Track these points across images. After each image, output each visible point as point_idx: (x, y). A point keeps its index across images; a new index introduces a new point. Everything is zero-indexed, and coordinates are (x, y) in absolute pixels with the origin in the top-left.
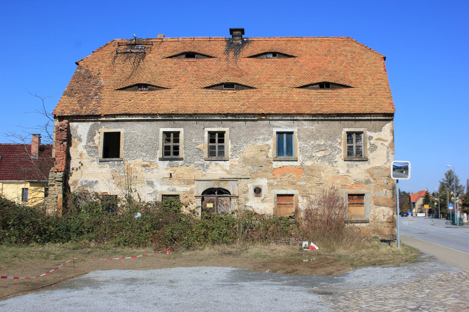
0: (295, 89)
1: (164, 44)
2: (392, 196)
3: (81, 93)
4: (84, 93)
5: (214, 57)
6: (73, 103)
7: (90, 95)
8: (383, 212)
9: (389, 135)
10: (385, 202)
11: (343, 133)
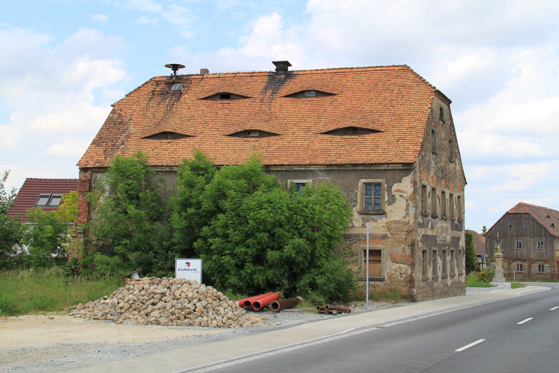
0: (320, 135)
1: (204, 81)
2: (410, 253)
3: (109, 142)
4: (111, 142)
5: (249, 98)
6: (98, 153)
7: (117, 144)
8: (401, 270)
9: (409, 187)
11: (360, 184)
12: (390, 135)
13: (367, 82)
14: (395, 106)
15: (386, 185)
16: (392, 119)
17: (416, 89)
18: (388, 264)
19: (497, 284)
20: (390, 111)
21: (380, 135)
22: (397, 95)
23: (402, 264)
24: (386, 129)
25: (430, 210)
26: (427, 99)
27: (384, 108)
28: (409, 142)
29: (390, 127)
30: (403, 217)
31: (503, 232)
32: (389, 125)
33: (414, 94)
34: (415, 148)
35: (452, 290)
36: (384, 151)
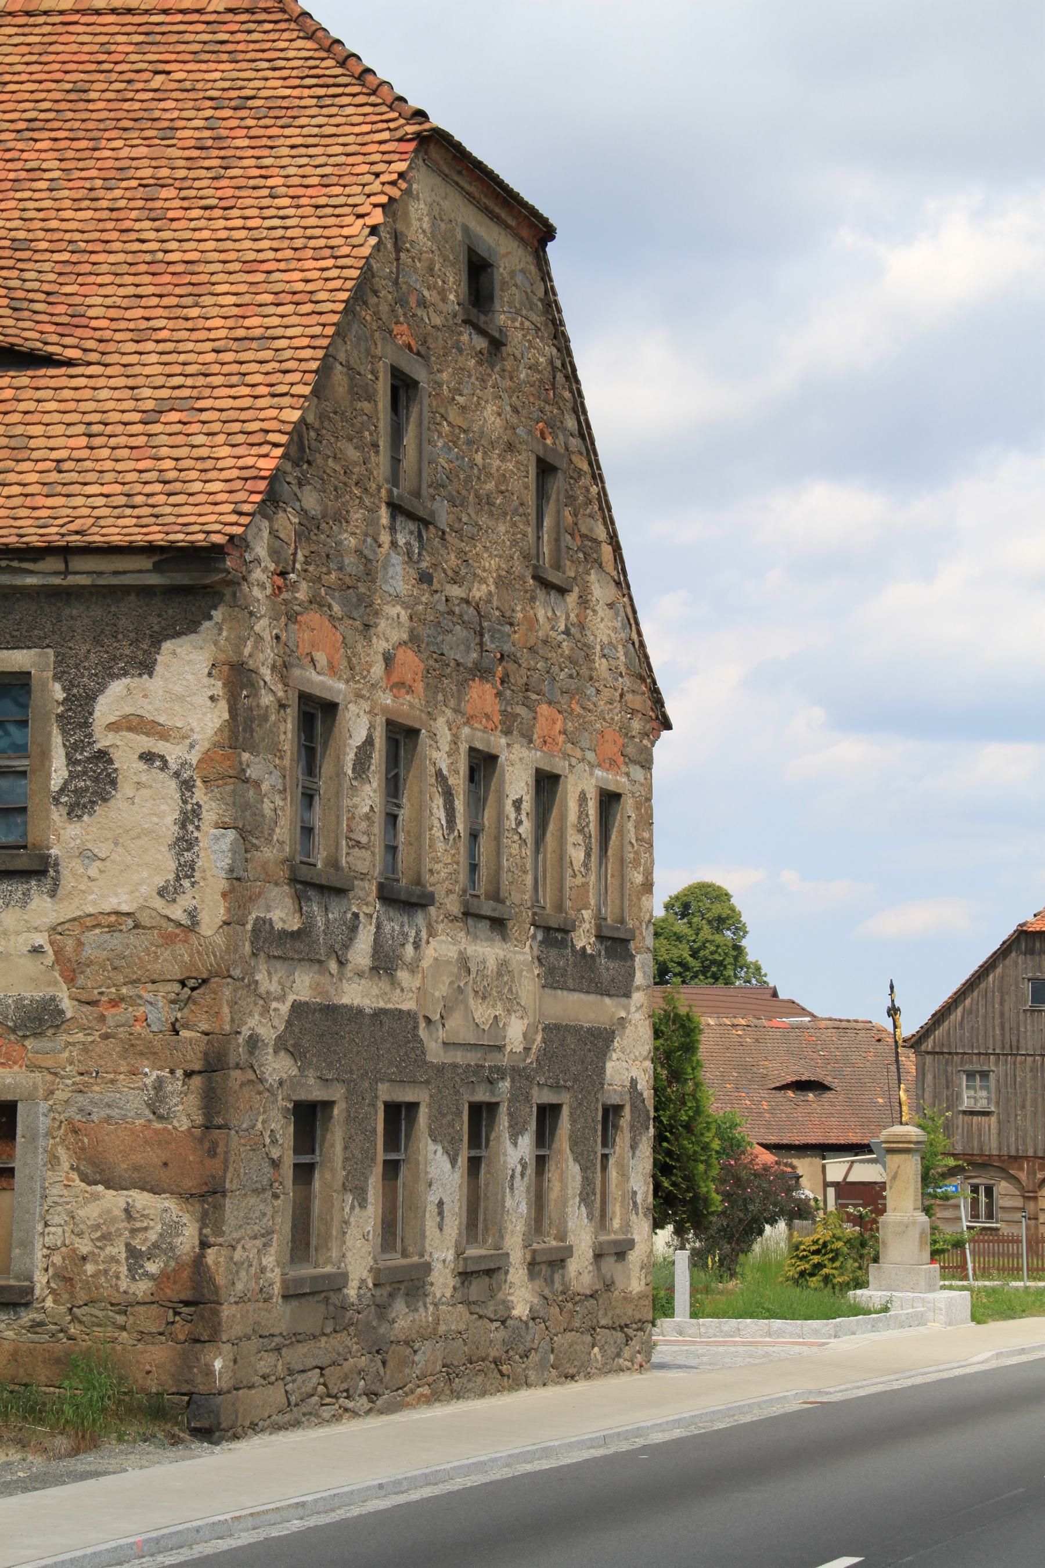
2: (199, 1119)
8: (134, 1231)
9: (202, 699)
10: (153, 1157)
12: (112, 382)
13: (24, 77)
14: (171, 214)
15: (57, 686)
16: (140, 291)
17: (314, 121)
18: (55, 1191)
19: (890, 1301)
20: (137, 246)
21: (53, 383)
22: (195, 153)
23: (142, 1189)
24: (91, 344)
25: (366, 854)
26: (370, 178)
27: (101, 226)
28: (216, 427)
29: (118, 336)
30: (161, 893)
31: (1003, 1029)
32: (115, 325)
33: (294, 152)
34: (250, 461)
35: (545, 1345)
36: (54, 476)
